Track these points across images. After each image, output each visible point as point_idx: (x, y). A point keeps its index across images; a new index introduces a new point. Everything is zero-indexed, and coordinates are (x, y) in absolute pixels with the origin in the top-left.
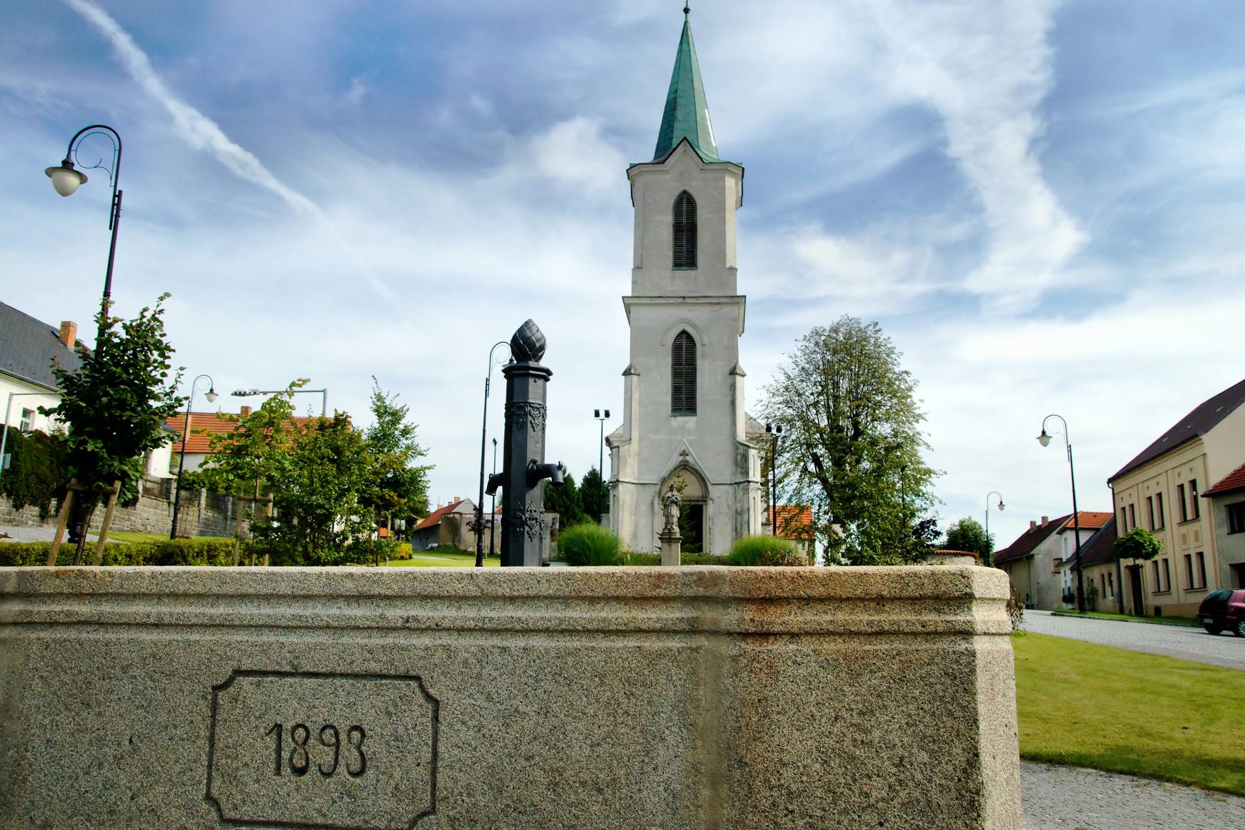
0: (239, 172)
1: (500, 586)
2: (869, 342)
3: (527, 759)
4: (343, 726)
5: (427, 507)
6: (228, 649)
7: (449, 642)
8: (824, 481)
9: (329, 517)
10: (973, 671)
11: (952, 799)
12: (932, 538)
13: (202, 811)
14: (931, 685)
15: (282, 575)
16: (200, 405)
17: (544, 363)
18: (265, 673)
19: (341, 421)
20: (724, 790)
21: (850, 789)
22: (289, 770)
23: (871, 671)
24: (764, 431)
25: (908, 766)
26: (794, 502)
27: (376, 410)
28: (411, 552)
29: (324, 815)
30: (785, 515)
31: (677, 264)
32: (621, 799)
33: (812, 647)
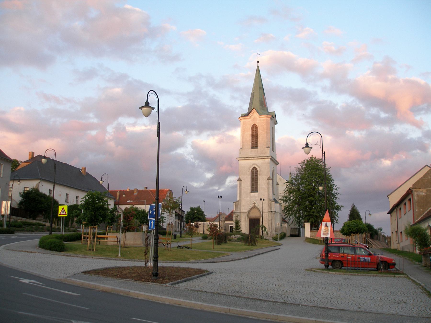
31: (253, 147)
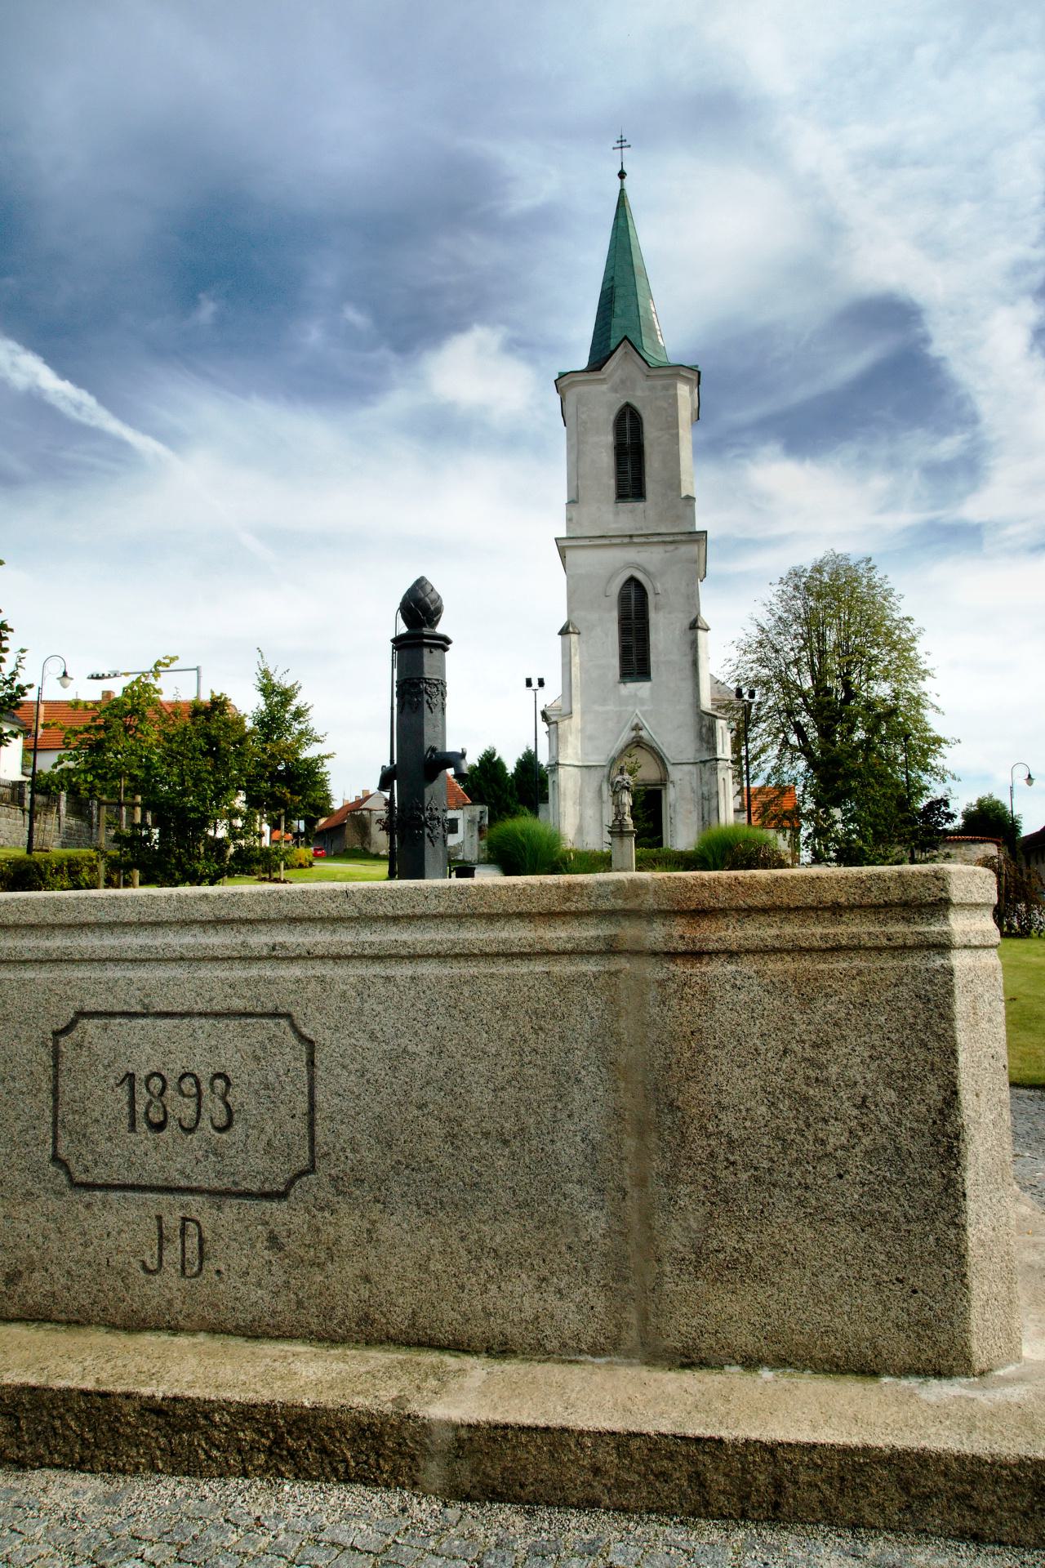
0: (74, 414)
1: (381, 904)
2: (860, 584)
3: (419, 1108)
4: (204, 1074)
5: (329, 803)
6: (68, 987)
7: (324, 973)
8: (809, 755)
9: (204, 821)
10: (950, 993)
11: (925, 1145)
12: (943, 821)
13: (50, 1174)
14: (899, 1010)
15: (125, 899)
16: (54, 692)
17: (440, 629)
18: (112, 1015)
19: (218, 705)
20: (653, 1140)
21: (803, 1136)
22: (145, 1126)
23: (826, 995)
24: (733, 696)
25: (873, 1108)
26: (773, 782)
27: (261, 690)
28: (311, 858)
29: (188, 1177)
30: (762, 798)
32: (530, 1152)
33: (755, 967)
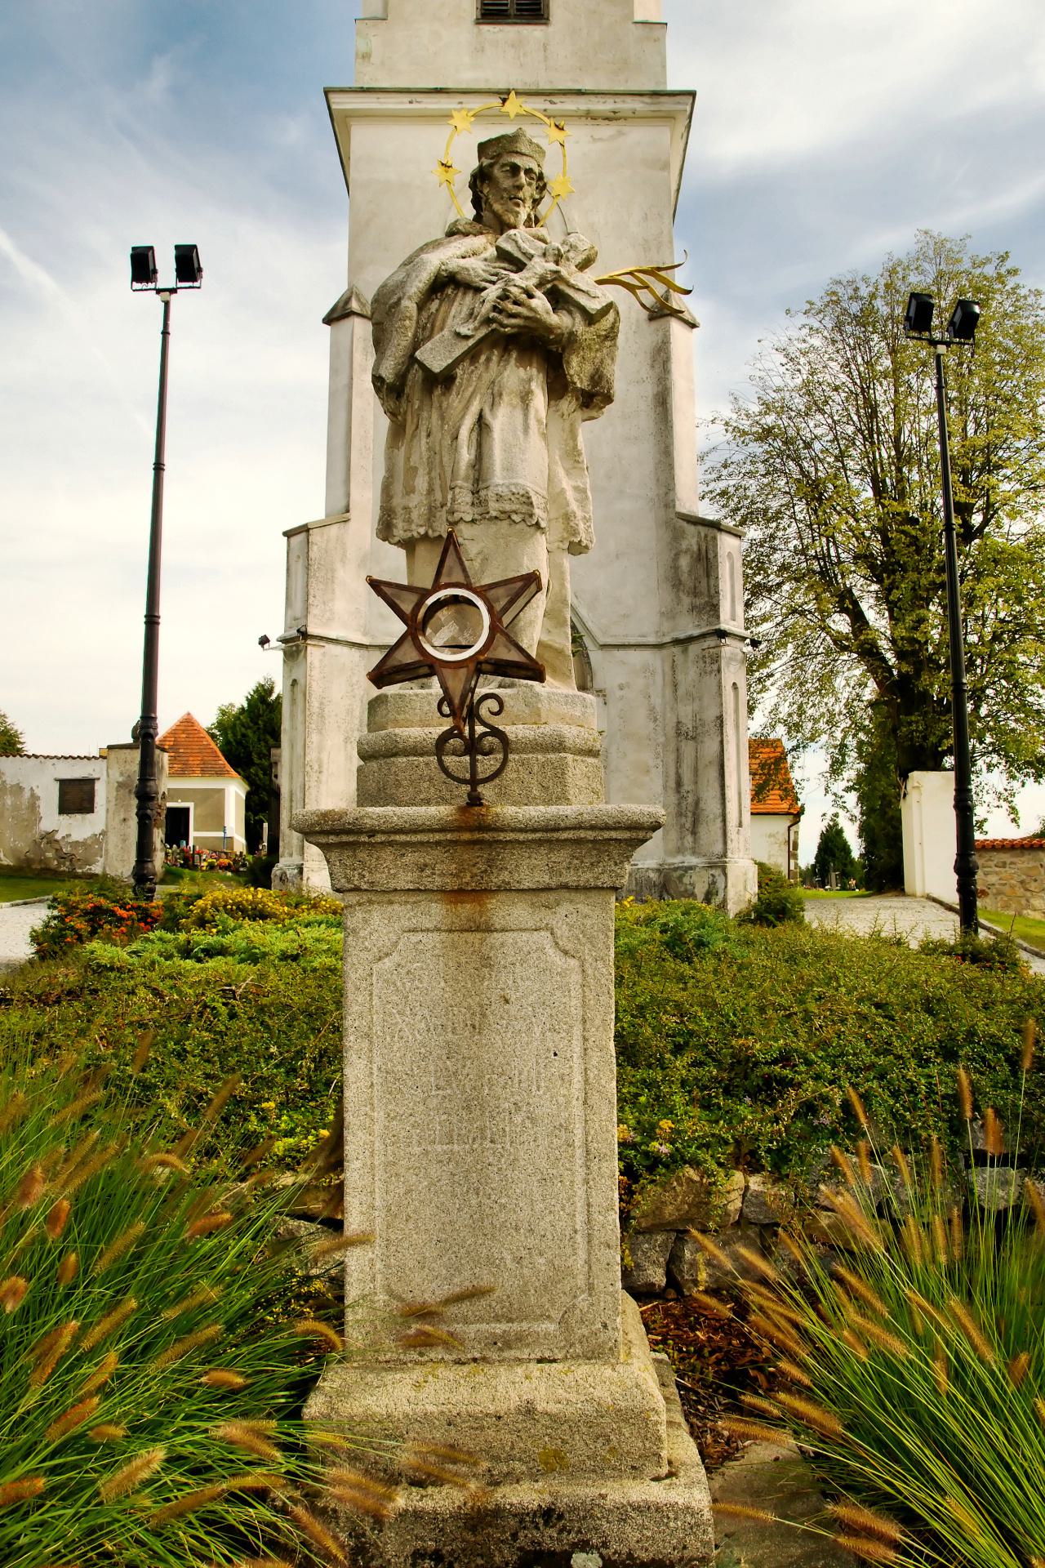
8: (869, 653)
